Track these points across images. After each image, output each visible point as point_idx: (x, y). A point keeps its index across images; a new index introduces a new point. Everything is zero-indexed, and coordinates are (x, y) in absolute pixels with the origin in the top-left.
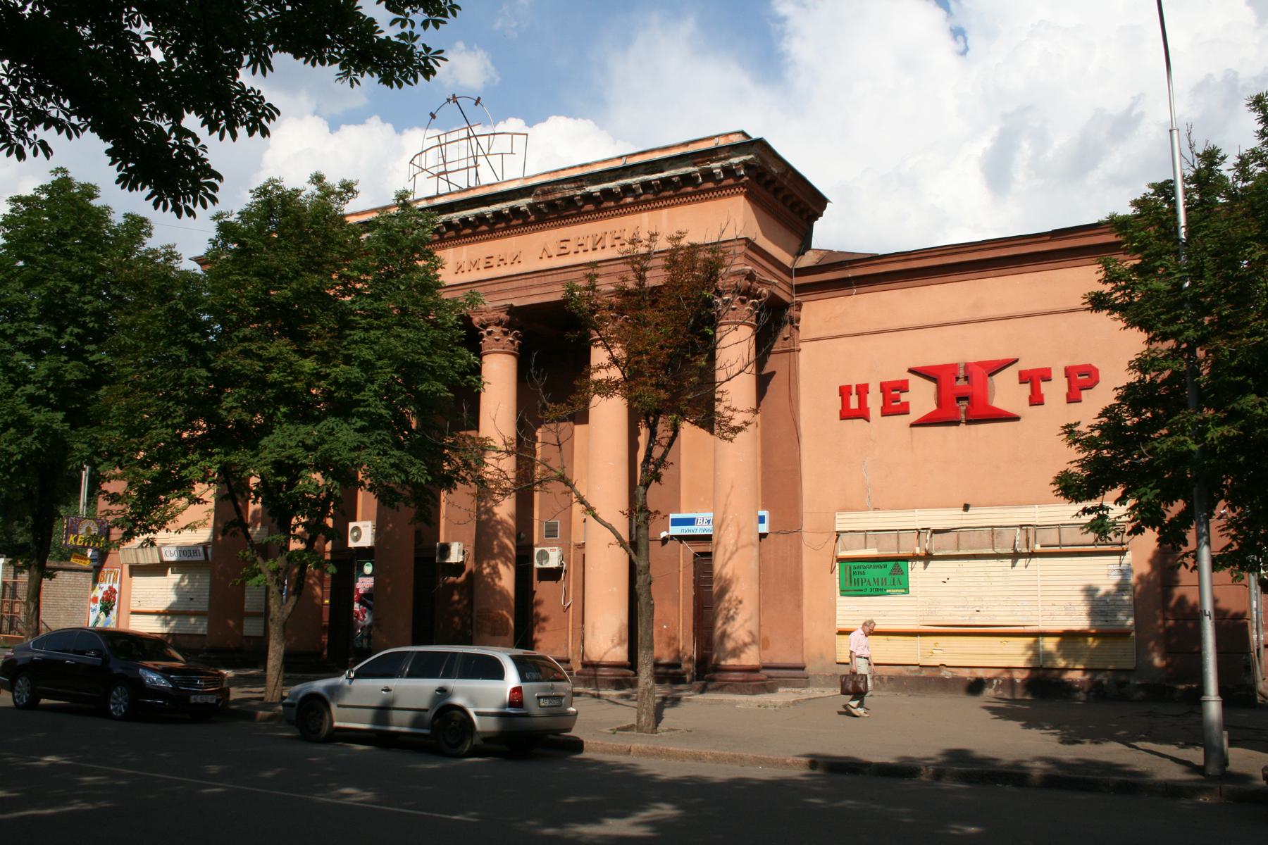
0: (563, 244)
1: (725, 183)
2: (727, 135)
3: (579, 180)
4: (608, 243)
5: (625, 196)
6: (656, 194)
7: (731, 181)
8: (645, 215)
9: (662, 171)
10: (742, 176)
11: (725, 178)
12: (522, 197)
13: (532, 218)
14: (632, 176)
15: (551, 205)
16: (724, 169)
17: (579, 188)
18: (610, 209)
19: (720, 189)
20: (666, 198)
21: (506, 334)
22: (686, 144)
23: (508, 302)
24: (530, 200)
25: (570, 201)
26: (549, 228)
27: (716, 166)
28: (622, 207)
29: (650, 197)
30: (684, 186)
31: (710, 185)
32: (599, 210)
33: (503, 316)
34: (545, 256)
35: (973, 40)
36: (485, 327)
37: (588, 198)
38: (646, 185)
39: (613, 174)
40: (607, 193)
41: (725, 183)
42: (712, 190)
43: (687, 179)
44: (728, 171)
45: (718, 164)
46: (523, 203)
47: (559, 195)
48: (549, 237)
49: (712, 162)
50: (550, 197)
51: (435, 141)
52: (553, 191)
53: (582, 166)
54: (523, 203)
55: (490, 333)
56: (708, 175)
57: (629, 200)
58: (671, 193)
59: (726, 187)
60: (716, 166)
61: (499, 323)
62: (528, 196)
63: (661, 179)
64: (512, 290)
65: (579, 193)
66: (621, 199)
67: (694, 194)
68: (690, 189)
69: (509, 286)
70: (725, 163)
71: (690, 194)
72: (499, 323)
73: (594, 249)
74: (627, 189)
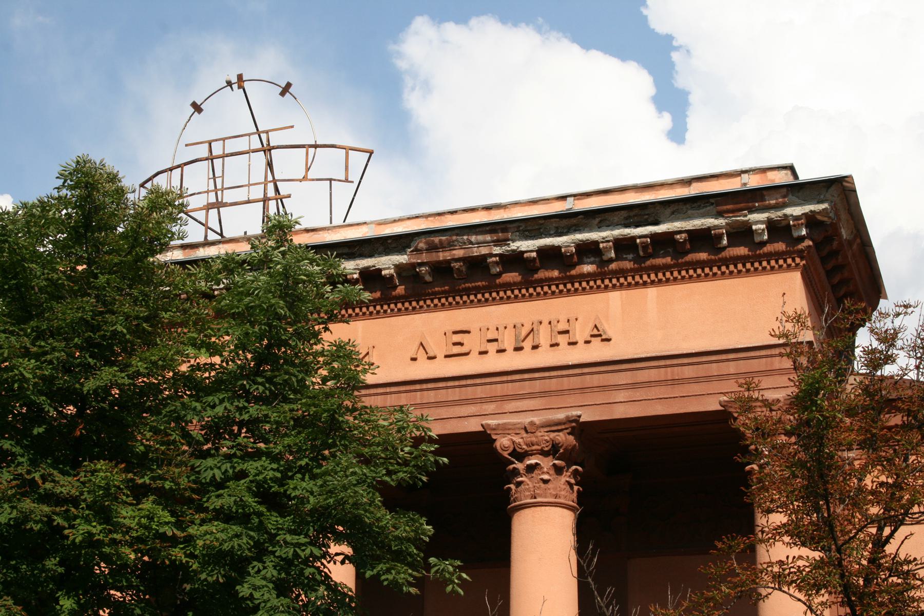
0: (457, 338)
1: (769, 248)
2: (764, 170)
3: (501, 230)
4: (544, 338)
5: (581, 262)
6: (638, 260)
7: (780, 246)
8: (615, 297)
9: (656, 223)
10: (802, 239)
11: (771, 240)
12: (387, 252)
13: (401, 290)
14: (600, 227)
15: (442, 270)
16: (770, 224)
17: (498, 243)
18: (549, 281)
19: (759, 258)
20: (656, 269)
21: (558, 470)
22: (688, 182)
23: (575, 412)
24: (402, 259)
25: (477, 265)
26: (429, 309)
27: (758, 220)
28: (572, 280)
29: (628, 265)
30: (694, 250)
31: (742, 251)
32: (528, 283)
33: (565, 439)
34: (421, 356)
35: (695, 122)
36: (520, 456)
37: (514, 260)
38: (624, 246)
39: (565, 222)
40: (549, 256)
41: (769, 248)
42: (743, 259)
43: (702, 238)
44: (778, 229)
45: (763, 216)
46: (387, 263)
47: (459, 253)
48: (432, 325)
49: (752, 211)
50: (442, 256)
51: (203, 151)
52: (450, 246)
53: (488, 208)
54: (387, 263)
55: (531, 469)
56: (742, 234)
57: (588, 268)
58: (668, 260)
59: (769, 256)
60: (758, 220)
61: (553, 450)
62: (400, 250)
63: (653, 236)
64: (531, 396)
65: (497, 250)
66: (573, 266)
67: (709, 264)
68: (703, 256)
69: (469, 392)
70: (774, 215)
71: (702, 264)
72: (553, 450)
73: (518, 349)
74: (588, 250)
